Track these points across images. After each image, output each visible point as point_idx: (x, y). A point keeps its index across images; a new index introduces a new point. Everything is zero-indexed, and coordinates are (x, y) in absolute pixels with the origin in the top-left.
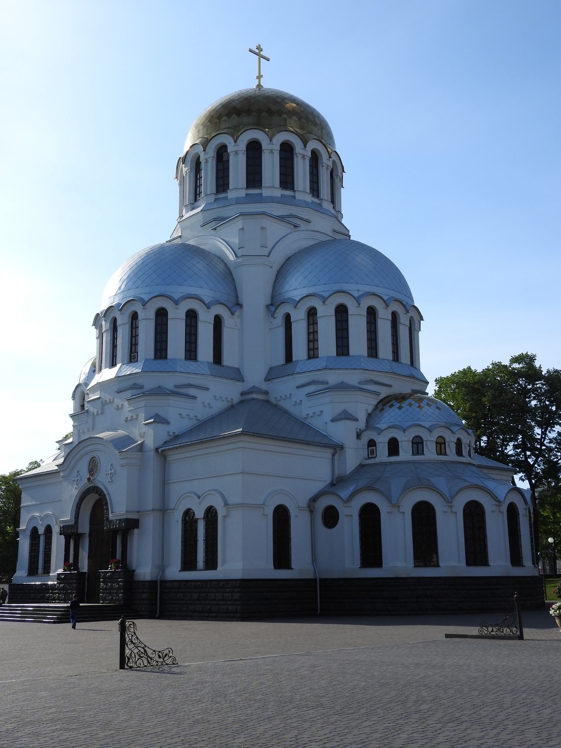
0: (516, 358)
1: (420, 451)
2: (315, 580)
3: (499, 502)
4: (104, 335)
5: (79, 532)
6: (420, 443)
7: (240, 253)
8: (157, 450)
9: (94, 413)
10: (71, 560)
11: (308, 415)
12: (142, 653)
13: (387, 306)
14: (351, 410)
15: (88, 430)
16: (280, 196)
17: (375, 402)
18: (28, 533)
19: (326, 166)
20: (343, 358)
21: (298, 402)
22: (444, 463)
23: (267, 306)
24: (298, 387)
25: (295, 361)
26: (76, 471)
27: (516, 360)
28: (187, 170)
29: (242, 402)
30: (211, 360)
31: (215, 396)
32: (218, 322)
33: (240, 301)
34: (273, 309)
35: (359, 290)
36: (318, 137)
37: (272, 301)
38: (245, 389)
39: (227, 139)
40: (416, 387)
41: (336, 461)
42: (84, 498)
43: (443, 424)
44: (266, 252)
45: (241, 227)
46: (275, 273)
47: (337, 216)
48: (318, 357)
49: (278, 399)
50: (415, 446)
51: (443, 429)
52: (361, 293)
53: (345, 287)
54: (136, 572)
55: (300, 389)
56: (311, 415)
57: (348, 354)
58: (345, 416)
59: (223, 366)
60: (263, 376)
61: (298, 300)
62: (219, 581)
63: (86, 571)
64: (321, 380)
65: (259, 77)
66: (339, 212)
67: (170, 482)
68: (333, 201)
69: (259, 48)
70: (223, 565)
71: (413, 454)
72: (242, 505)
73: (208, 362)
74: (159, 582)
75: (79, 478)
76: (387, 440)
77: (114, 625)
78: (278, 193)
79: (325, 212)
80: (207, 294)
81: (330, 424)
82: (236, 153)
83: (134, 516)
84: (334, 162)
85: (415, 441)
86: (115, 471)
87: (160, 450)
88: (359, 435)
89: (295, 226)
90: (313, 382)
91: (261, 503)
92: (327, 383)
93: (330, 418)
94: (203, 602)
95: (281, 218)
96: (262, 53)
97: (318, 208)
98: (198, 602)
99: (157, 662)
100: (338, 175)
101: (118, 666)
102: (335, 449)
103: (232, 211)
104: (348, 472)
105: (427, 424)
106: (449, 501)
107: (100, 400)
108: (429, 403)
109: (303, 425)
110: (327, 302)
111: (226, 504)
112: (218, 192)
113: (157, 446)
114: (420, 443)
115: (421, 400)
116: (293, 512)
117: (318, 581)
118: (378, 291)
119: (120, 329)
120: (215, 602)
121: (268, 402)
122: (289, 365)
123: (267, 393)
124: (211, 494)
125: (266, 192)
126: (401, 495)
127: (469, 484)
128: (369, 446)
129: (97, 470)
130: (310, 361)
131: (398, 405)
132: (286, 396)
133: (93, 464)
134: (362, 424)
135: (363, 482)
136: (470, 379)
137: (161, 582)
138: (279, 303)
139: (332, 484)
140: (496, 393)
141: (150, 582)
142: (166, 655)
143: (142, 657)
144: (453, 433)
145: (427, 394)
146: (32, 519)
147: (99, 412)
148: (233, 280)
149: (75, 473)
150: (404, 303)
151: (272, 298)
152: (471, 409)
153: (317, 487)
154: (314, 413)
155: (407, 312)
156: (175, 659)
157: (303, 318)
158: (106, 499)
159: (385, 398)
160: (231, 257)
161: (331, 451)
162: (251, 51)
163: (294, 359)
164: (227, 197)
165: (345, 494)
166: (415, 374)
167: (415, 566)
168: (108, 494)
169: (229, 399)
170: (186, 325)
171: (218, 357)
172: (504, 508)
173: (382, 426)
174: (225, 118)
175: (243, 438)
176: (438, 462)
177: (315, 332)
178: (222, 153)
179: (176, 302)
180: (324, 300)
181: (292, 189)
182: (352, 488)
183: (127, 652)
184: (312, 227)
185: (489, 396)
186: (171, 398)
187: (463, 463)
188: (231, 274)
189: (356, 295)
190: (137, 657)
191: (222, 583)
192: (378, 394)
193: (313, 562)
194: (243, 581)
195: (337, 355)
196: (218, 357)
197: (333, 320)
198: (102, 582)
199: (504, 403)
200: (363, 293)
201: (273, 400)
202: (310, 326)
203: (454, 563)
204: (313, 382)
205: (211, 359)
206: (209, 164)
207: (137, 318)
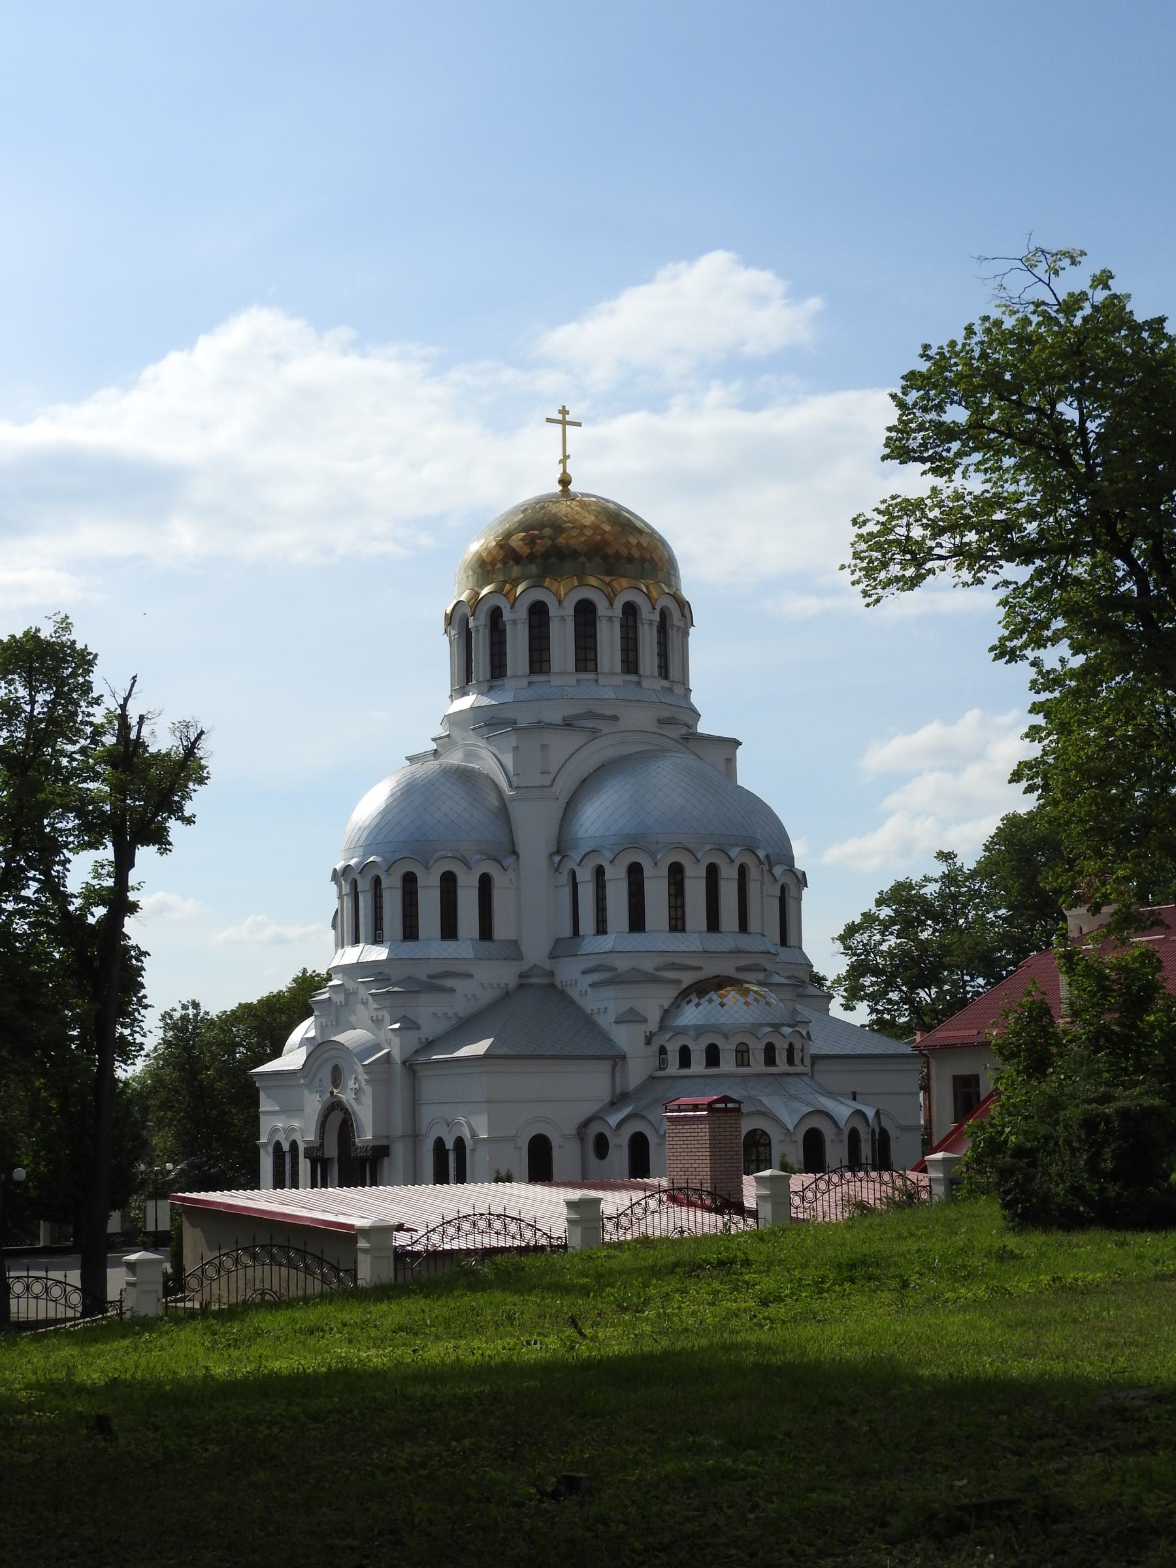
4: (345, 898)
5: (326, 1156)
7: (515, 780)
18: (270, 1149)
22: (744, 1077)
24: (583, 973)
26: (318, 1079)
29: (521, 986)
30: (477, 936)
31: (482, 984)
32: (485, 883)
37: (558, 847)
41: (618, 1074)
58: (632, 1017)
65: (563, 461)
68: (664, 670)
69: (564, 412)
83: (383, 1143)
88: (648, 1042)
92: (615, 969)
96: (568, 418)
113: (404, 1058)
116: (555, 1142)
128: (660, 1054)
134: (653, 1024)
149: (317, 1082)
171: (486, 932)
182: (626, 1112)
192: (679, 982)
196: (486, 932)
201: (559, 985)
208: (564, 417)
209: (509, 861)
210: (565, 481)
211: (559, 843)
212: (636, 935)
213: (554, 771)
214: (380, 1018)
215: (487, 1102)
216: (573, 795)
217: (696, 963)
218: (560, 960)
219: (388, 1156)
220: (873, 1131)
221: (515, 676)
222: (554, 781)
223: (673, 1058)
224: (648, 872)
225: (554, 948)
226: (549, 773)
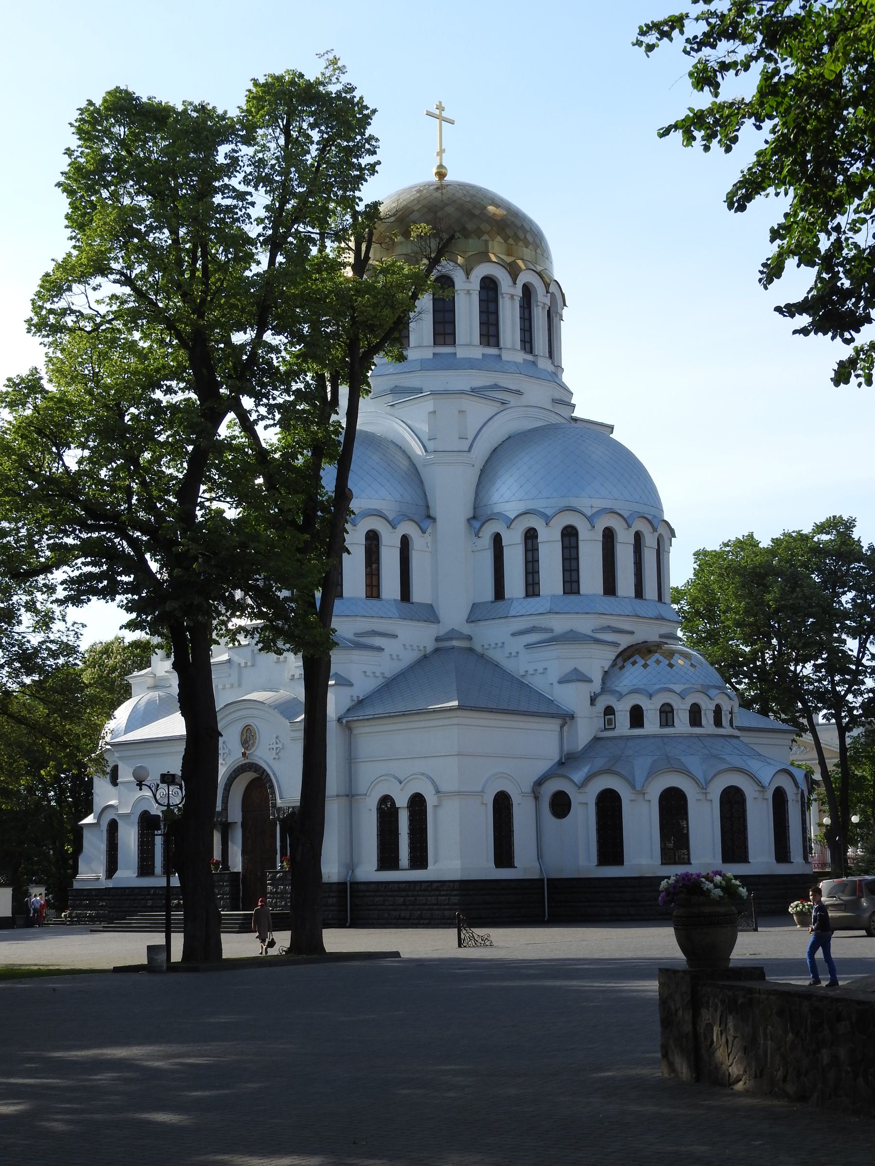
0: (823, 524)
1: (670, 723)
2: (541, 880)
5: (229, 821)
6: (670, 712)
7: (431, 446)
8: (339, 720)
9: (240, 664)
13: (629, 526)
15: (232, 686)
16: (480, 357)
19: (542, 305)
20: (572, 598)
21: (514, 654)
22: (699, 736)
23: (469, 520)
24: (513, 635)
27: (821, 528)
29: (437, 650)
32: (405, 543)
33: (432, 514)
34: (477, 524)
35: (593, 505)
38: (442, 633)
41: (565, 734)
42: (235, 778)
43: (699, 687)
44: (465, 445)
48: (539, 595)
49: (485, 647)
50: (664, 715)
52: (595, 510)
53: (575, 503)
56: (531, 672)
57: (578, 592)
58: (577, 677)
59: (413, 603)
60: (465, 616)
62: (431, 882)
63: (240, 870)
64: (543, 626)
65: (441, 152)
67: (358, 760)
68: (551, 355)
69: (440, 107)
72: (459, 793)
73: (395, 600)
74: (348, 884)
78: (478, 352)
80: (388, 507)
81: (556, 685)
86: (283, 744)
87: (344, 721)
88: (593, 701)
91: (480, 790)
92: (551, 631)
94: (410, 907)
96: (444, 114)
98: (404, 907)
104: (580, 748)
105: (678, 688)
106: (703, 787)
109: (521, 686)
110: (551, 524)
111: (438, 792)
116: (516, 799)
117: (546, 882)
120: (427, 907)
121: (471, 650)
122: (500, 603)
123: (469, 638)
124: (417, 778)
125: (461, 353)
126: (646, 780)
129: (254, 743)
130: (530, 600)
131: (643, 662)
132: (497, 644)
133: (248, 735)
134: (597, 686)
135: (599, 763)
136: (747, 562)
137: (351, 883)
139: (561, 763)
140: (786, 586)
141: (339, 884)
144: (711, 699)
146: (138, 803)
147: (249, 664)
148: (422, 482)
150: (650, 517)
152: (747, 612)
153: (542, 767)
154: (536, 670)
158: (271, 780)
160: (418, 450)
162: (429, 114)
163: (506, 596)
165: (578, 776)
167: (662, 864)
169: (422, 648)
170: (563, 548)
172: (770, 794)
175: (460, 713)
176: (691, 736)
180: (547, 519)
181: (497, 345)
183: (462, 936)
184: (525, 400)
185: (775, 592)
186: (354, 652)
187: (722, 736)
189: (589, 514)
191: (435, 885)
192: (615, 644)
193: (538, 859)
197: (559, 546)
198: (269, 884)
199: (799, 604)
200: (598, 509)
201: (478, 648)
202: (528, 552)
203: (708, 860)
208: (441, 113)
209: (426, 523)
210: (441, 175)
211: (475, 508)
213: (471, 437)
215: (459, 755)
217: (627, 627)
218: (481, 623)
220: (802, 791)
223: (623, 719)
224: (543, 534)
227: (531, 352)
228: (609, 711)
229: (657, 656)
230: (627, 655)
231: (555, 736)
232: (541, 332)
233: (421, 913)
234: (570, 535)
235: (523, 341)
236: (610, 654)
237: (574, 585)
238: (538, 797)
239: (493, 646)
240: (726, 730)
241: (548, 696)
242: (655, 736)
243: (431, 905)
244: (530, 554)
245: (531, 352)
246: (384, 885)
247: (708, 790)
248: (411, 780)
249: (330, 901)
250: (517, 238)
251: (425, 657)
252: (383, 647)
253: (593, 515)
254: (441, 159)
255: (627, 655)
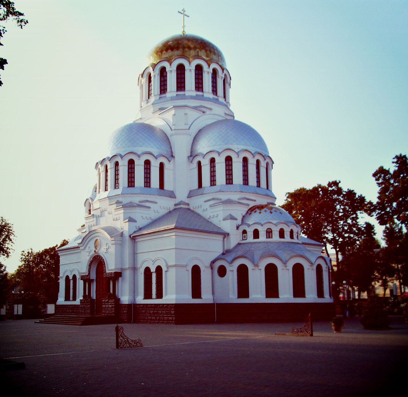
2: (213, 304)
3: (312, 264)
7: (173, 128)
10: (87, 294)
11: (210, 216)
12: (126, 341)
13: (254, 157)
14: (235, 215)
16: (195, 95)
17: (247, 210)
22: (283, 243)
23: (188, 157)
24: (205, 202)
25: (204, 187)
28: (144, 81)
29: (175, 209)
30: (158, 187)
32: (162, 166)
34: (191, 158)
35: (239, 148)
36: (216, 61)
38: (177, 202)
39: (166, 64)
40: (270, 201)
41: (225, 242)
44: (187, 127)
45: (173, 113)
46: (193, 138)
47: (226, 105)
48: (216, 185)
51: (283, 225)
52: (239, 150)
53: (230, 147)
54: (120, 299)
55: (206, 203)
58: (232, 218)
59: (165, 190)
60: (187, 195)
61: (205, 154)
62: (164, 304)
65: (184, 27)
66: (228, 103)
68: (225, 97)
70: (165, 296)
71: (267, 238)
72: (175, 266)
73: (157, 188)
75: (90, 250)
76: (252, 230)
77: (112, 327)
78: (194, 93)
79: (221, 104)
80: (156, 152)
81: (222, 222)
82: (171, 71)
84: (225, 75)
85: (268, 231)
87: (132, 236)
88: (238, 228)
89: (204, 112)
90: (213, 199)
92: (221, 199)
93: (222, 218)
95: (195, 108)
96: (185, 13)
97: (216, 101)
99: (134, 345)
100: (227, 82)
101: (115, 347)
102: (225, 235)
103: (170, 105)
105: (274, 222)
107: (100, 209)
108: (276, 210)
112: (161, 93)
113: (130, 234)
114: (270, 232)
115: (272, 208)
117: (215, 305)
118: (249, 148)
119: (109, 171)
121: (189, 209)
122: (201, 189)
123: (188, 204)
126: (260, 259)
127: (296, 254)
128: (243, 234)
130: (211, 187)
132: (199, 206)
134: (239, 222)
138: (195, 155)
139: (223, 254)
142: (138, 342)
143: (126, 343)
145: (275, 205)
148: (170, 143)
150: (264, 155)
151: (191, 152)
154: (214, 216)
155: (265, 160)
156: (142, 344)
157: (208, 164)
158: (104, 261)
159: (252, 207)
161: (222, 236)
164: (166, 96)
165: (230, 259)
166: (269, 194)
167: (266, 297)
168: (105, 259)
169: (168, 208)
172: (315, 267)
173: (250, 223)
174: (164, 52)
176: (280, 242)
177: (214, 171)
178: (163, 71)
179: (139, 156)
180: (219, 154)
181: (202, 91)
184: (213, 112)
188: (169, 139)
189: (237, 151)
190: (124, 343)
192: (248, 205)
194: (176, 305)
195: (226, 184)
201: (192, 208)
204: (213, 199)
205: (158, 186)
206: (156, 77)
207: (118, 165)
212: (229, 186)
214: (118, 218)
216: (196, 135)
219: (121, 277)
221: (171, 92)
222: (190, 128)
223: (250, 234)
225: (189, 194)
226: (188, 125)
227: (216, 95)
228: (245, 232)
229: (265, 209)
230: (252, 210)
231: (221, 243)
232: (220, 88)
233: (160, 318)
234: (229, 160)
235: (213, 91)
236: (246, 209)
237: (231, 181)
238: (213, 268)
239: (197, 207)
240: (295, 240)
241: (218, 226)
242: (264, 242)
243: (163, 314)
244: (212, 169)
245: (216, 95)
246: (146, 305)
247: (287, 265)
248: (157, 260)
249: (125, 312)
250: (210, 51)
251: (170, 212)
252: (150, 207)
253: (239, 152)
254: (184, 29)
255: (252, 210)
